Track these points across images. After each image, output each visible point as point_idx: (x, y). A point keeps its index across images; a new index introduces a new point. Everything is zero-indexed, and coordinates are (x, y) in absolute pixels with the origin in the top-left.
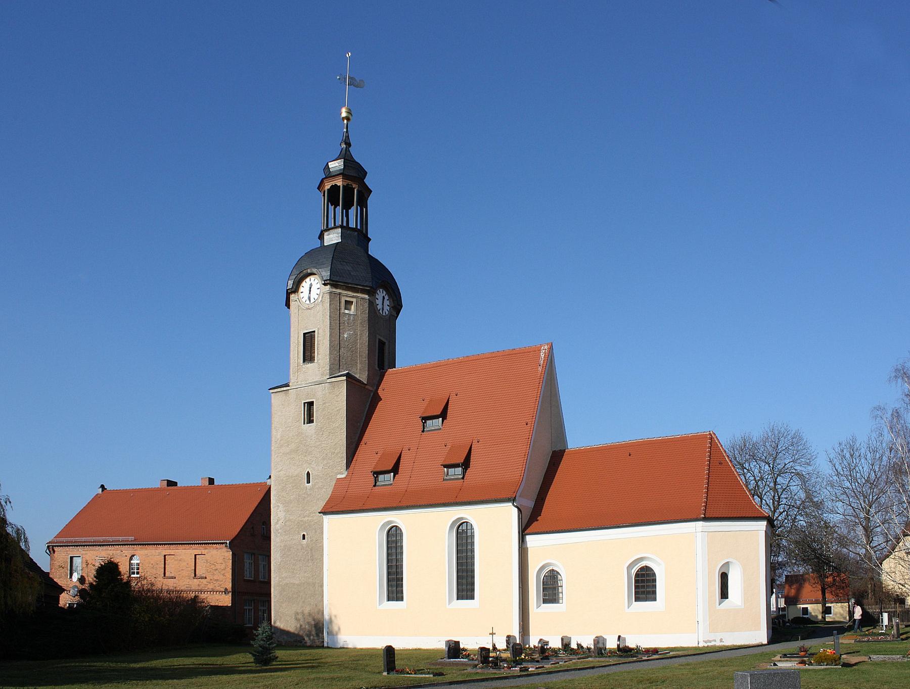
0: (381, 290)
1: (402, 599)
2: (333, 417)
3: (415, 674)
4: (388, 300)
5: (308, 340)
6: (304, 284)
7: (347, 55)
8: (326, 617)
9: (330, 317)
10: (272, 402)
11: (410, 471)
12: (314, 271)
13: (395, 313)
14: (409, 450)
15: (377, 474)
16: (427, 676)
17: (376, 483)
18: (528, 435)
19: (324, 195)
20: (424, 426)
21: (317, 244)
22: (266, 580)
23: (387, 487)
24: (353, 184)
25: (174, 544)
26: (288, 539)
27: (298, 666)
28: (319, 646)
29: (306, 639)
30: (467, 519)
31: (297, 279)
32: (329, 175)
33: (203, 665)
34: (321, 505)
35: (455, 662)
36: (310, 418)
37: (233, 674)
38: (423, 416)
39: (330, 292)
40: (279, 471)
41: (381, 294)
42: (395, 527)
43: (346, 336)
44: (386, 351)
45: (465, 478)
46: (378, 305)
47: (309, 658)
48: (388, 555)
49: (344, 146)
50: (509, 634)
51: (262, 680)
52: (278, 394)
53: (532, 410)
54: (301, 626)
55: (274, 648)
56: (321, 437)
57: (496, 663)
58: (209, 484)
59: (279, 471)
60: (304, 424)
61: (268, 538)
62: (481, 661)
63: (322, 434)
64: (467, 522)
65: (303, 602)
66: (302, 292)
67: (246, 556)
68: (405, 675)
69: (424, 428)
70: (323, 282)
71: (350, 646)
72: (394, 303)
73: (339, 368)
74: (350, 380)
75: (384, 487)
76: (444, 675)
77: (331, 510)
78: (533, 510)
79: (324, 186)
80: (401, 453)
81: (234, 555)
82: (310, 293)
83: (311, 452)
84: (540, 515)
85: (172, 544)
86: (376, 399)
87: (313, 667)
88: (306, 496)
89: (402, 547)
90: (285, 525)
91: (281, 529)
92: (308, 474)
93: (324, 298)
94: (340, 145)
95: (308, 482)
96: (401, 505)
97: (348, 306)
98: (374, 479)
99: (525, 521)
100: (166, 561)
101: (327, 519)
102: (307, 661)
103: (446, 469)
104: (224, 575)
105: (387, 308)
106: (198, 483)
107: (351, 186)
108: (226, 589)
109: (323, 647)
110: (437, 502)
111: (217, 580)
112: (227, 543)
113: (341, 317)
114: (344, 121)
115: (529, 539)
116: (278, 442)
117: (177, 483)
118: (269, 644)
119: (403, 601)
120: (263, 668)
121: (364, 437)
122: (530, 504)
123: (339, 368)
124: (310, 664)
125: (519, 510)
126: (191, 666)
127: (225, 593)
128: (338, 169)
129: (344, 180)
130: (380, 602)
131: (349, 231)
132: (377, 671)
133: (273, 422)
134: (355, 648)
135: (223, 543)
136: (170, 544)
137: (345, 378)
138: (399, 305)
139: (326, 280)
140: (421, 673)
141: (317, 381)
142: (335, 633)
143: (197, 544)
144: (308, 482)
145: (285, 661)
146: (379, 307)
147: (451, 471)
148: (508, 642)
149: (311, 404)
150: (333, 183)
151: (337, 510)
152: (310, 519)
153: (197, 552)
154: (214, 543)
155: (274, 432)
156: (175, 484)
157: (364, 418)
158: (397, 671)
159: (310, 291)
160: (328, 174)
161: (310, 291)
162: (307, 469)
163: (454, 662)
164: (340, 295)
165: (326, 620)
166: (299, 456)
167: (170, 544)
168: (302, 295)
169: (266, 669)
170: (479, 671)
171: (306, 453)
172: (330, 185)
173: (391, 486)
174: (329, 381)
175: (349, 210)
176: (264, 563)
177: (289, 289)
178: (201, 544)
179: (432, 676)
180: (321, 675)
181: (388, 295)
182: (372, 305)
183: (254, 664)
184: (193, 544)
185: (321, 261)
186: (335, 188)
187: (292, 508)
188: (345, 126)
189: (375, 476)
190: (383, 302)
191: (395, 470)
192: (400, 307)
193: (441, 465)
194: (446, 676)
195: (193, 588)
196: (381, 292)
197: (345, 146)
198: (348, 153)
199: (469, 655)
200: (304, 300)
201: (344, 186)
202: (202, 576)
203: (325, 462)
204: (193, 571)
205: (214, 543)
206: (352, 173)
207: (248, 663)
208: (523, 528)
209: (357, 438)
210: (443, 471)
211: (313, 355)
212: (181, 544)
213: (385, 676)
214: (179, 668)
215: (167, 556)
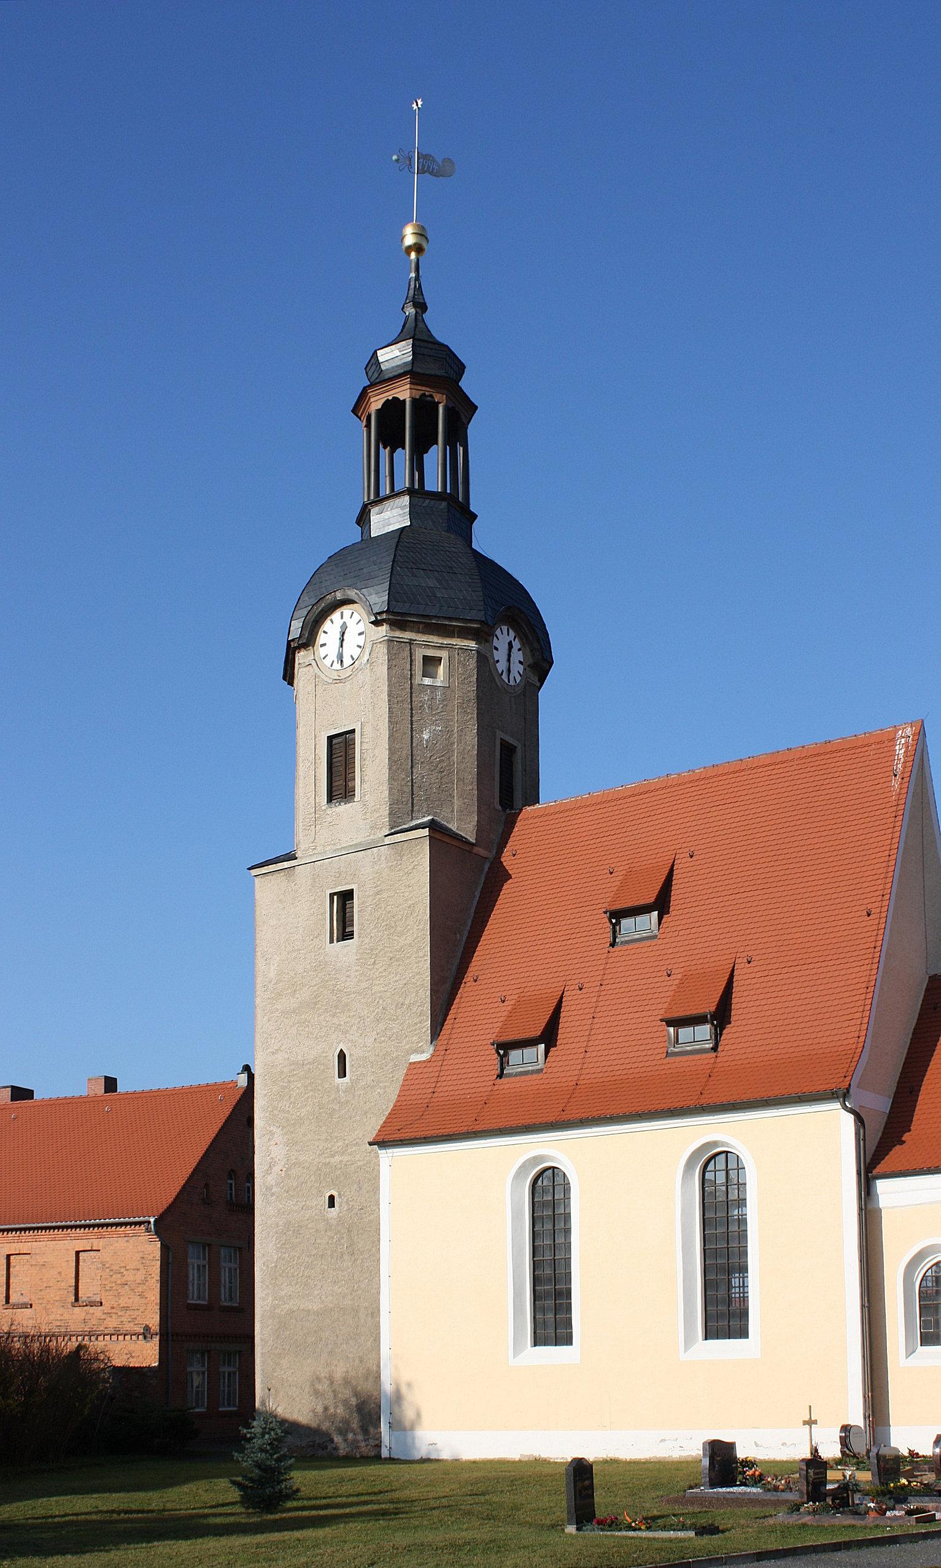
0: (505, 628)
1: (568, 1340)
2: (397, 924)
3: (648, 1528)
4: (519, 650)
5: (339, 752)
6: (327, 626)
7: (414, 105)
8: (387, 1386)
9: (389, 695)
10: (257, 897)
11: (586, 1038)
12: (352, 593)
13: (535, 680)
14: (581, 989)
15: (505, 1047)
16: (681, 1534)
17: (502, 1069)
18: (873, 939)
19: (368, 426)
20: (614, 932)
21: (354, 535)
22: (237, 1305)
23: (529, 1077)
24: (434, 395)
25: (30, 1229)
26: (294, 1208)
27: (347, 1510)
28: (368, 1457)
29: (337, 1439)
30: (723, 1144)
31: (312, 617)
32: (378, 378)
33: (119, 1513)
34: (373, 1126)
35: (732, 1496)
36: (344, 928)
37: (202, 1536)
38: (613, 908)
39: (388, 640)
40: (273, 1053)
41: (504, 637)
42: (551, 1171)
43: (426, 737)
44: (518, 767)
45: (719, 1049)
46: (498, 661)
47: (362, 1488)
48: (534, 1235)
49: (410, 311)
50: (846, 1423)
51: (282, 1554)
52: (270, 877)
53: (879, 882)
54: (326, 1409)
55: (290, 1468)
56: (371, 970)
57: (843, 1498)
58: (105, 1093)
59: (273, 1053)
60: (332, 941)
61: (246, 1208)
62: (808, 1493)
63: (374, 963)
64: (727, 1152)
65: (331, 1353)
66: (324, 645)
67: (191, 1249)
68: (624, 1533)
69: (615, 938)
70: (373, 619)
71: (445, 1455)
72: (533, 655)
73: (412, 811)
74: (438, 836)
75: (698, 1056)
76: (723, 1532)
77: (397, 1136)
78: (888, 1117)
79: (368, 404)
80: (562, 997)
81: (165, 1249)
82: (342, 646)
83: (347, 1005)
84: (910, 1130)
85: (25, 1229)
86: (497, 877)
87: (384, 1513)
88: (337, 1107)
89: (567, 1217)
90: (288, 1176)
91: (277, 1185)
92: (342, 1056)
93: (374, 655)
94: (403, 309)
95: (342, 1073)
96: (564, 1117)
97: (430, 669)
98: (497, 1062)
99: (872, 1146)
100: (11, 1269)
101: (388, 1157)
102: (363, 1498)
103: (671, 1029)
104: (141, 1296)
105: (517, 668)
106: (81, 1089)
107: (429, 399)
108: (147, 1328)
109: (377, 1458)
110: (659, 1107)
111: (126, 1308)
112: (149, 1222)
113: (414, 695)
114: (409, 255)
115: (882, 1186)
116: (271, 986)
117: (32, 1092)
118: (278, 1460)
119: (571, 1344)
120: (265, 1517)
121: (472, 964)
122: (880, 1104)
123: (412, 811)
124: (376, 1507)
125: (859, 1120)
126: (94, 1517)
127: (145, 1338)
128: (399, 363)
129: (413, 387)
130: (517, 1349)
131: (427, 501)
132: (548, 1522)
133: (258, 941)
134: (458, 1460)
135: (140, 1223)
136: (21, 1230)
137: (426, 832)
138: (545, 660)
139: (380, 613)
140: (664, 1528)
141: (360, 844)
142: (407, 1424)
143: (80, 1227)
144: (342, 1073)
145: (310, 1499)
146: (501, 666)
147: (685, 1033)
148: (844, 1442)
149: (346, 897)
150: (389, 396)
151: (412, 1135)
152: (346, 1158)
153: (80, 1245)
154: (121, 1224)
155: (260, 965)
156: (27, 1094)
157: (469, 923)
158: (600, 1522)
159: (342, 641)
160: (376, 375)
161: (342, 641)
162: (339, 1043)
163: (728, 1496)
164: (410, 644)
165: (386, 1396)
166: (319, 1015)
167: (21, 1230)
168: (322, 651)
169: (276, 1521)
170: (807, 1519)
171: (336, 1007)
172: (383, 400)
173: (540, 1075)
174: (388, 840)
175: (425, 455)
176: (232, 1265)
177: (293, 640)
178: (89, 1226)
179: (692, 1534)
180: (421, 1536)
181: (521, 640)
182: (484, 661)
183: (238, 1509)
184: (71, 1227)
185: (365, 571)
186: (393, 407)
187: (304, 1135)
188: (413, 266)
189: (502, 1052)
190: (509, 656)
191: (549, 1036)
192: (546, 665)
193: (662, 1020)
194: (727, 1534)
195: (73, 1327)
196: (505, 632)
197: (413, 311)
198: (420, 325)
199: (761, 1477)
200: (328, 662)
201: (414, 401)
202: (93, 1299)
203: (382, 1026)
204: (72, 1289)
205: (121, 1224)
206: (432, 369)
207: (223, 1505)
208: (868, 1161)
209: (454, 968)
210: (665, 1033)
211: (350, 784)
212: (46, 1228)
213: (571, 1535)
214: (65, 1522)
215: (12, 1257)
